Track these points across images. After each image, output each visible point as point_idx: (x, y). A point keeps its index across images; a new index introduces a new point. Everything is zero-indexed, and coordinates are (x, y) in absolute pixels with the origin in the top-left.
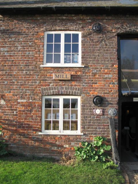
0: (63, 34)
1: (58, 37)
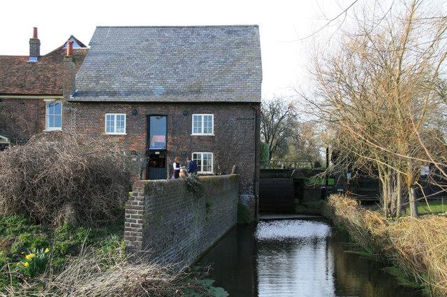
0: (116, 115)
1: (205, 132)
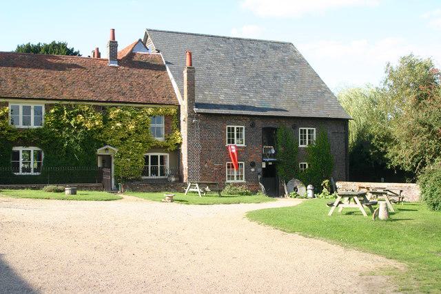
0: (235, 127)
